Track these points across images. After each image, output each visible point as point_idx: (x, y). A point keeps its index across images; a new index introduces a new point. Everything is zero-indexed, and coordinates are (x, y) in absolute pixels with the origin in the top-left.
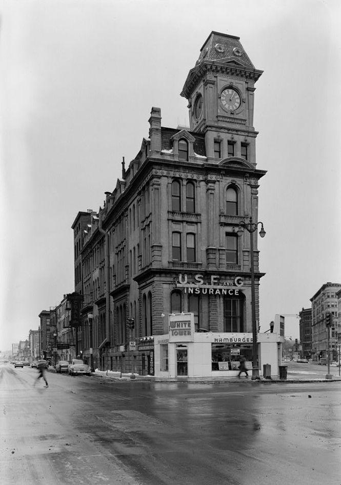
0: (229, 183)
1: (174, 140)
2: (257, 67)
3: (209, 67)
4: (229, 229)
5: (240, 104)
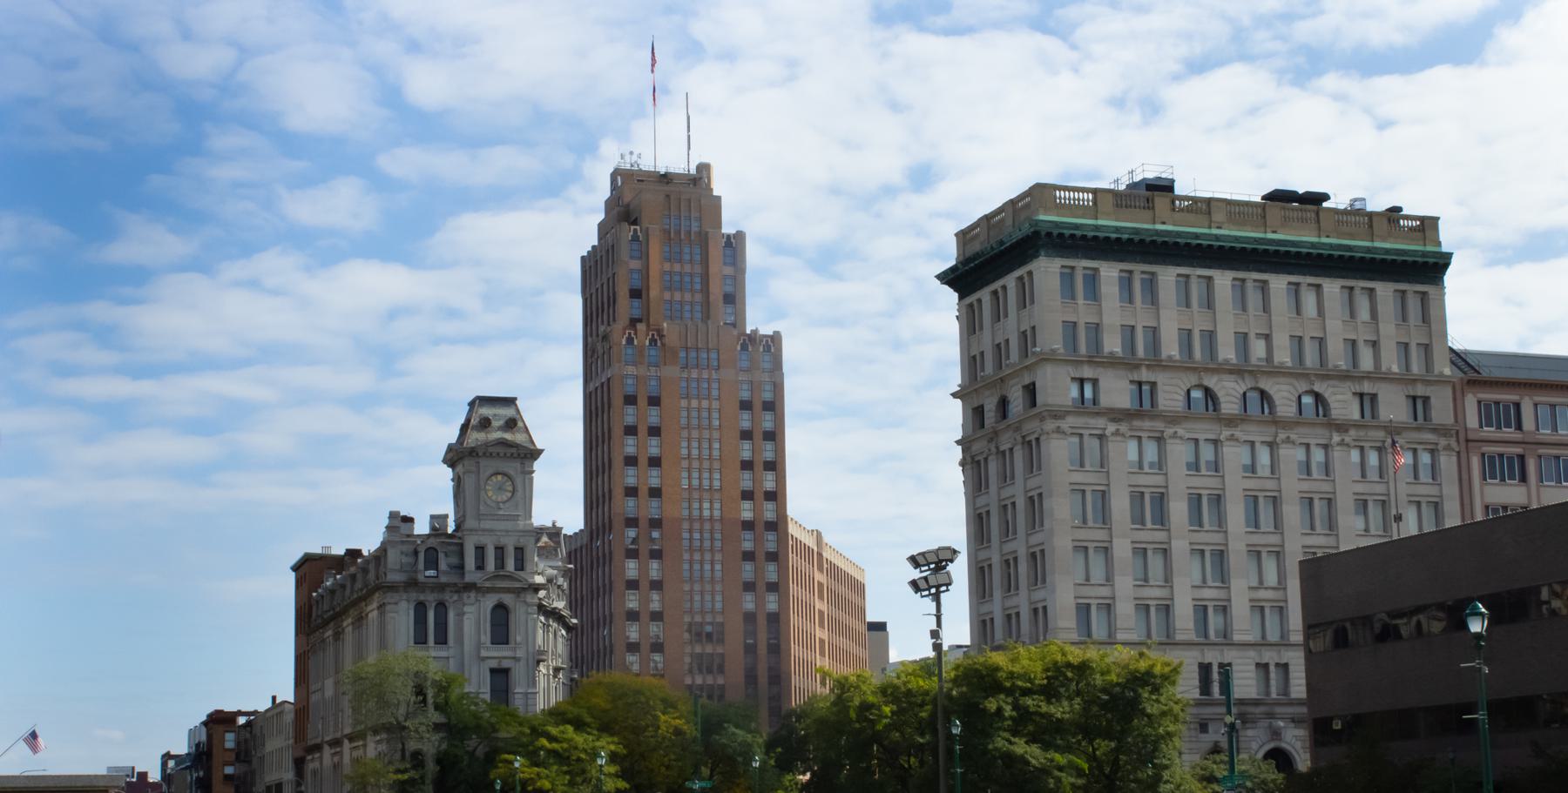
2: (539, 446)
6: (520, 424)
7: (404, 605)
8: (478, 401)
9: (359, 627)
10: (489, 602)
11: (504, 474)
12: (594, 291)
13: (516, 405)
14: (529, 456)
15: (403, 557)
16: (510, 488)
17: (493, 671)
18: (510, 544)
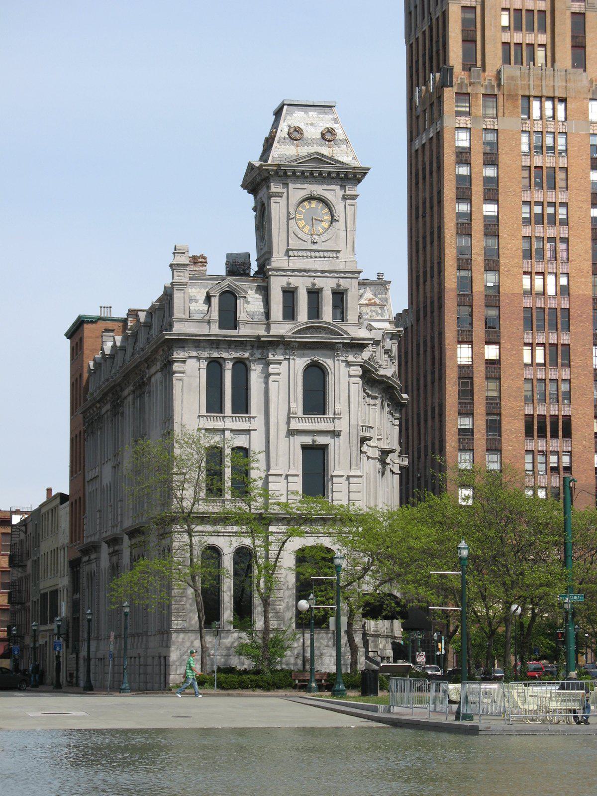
9: (140, 396)
10: (300, 363)
12: (420, 35)
16: (328, 217)
17: (305, 447)
18: (327, 285)
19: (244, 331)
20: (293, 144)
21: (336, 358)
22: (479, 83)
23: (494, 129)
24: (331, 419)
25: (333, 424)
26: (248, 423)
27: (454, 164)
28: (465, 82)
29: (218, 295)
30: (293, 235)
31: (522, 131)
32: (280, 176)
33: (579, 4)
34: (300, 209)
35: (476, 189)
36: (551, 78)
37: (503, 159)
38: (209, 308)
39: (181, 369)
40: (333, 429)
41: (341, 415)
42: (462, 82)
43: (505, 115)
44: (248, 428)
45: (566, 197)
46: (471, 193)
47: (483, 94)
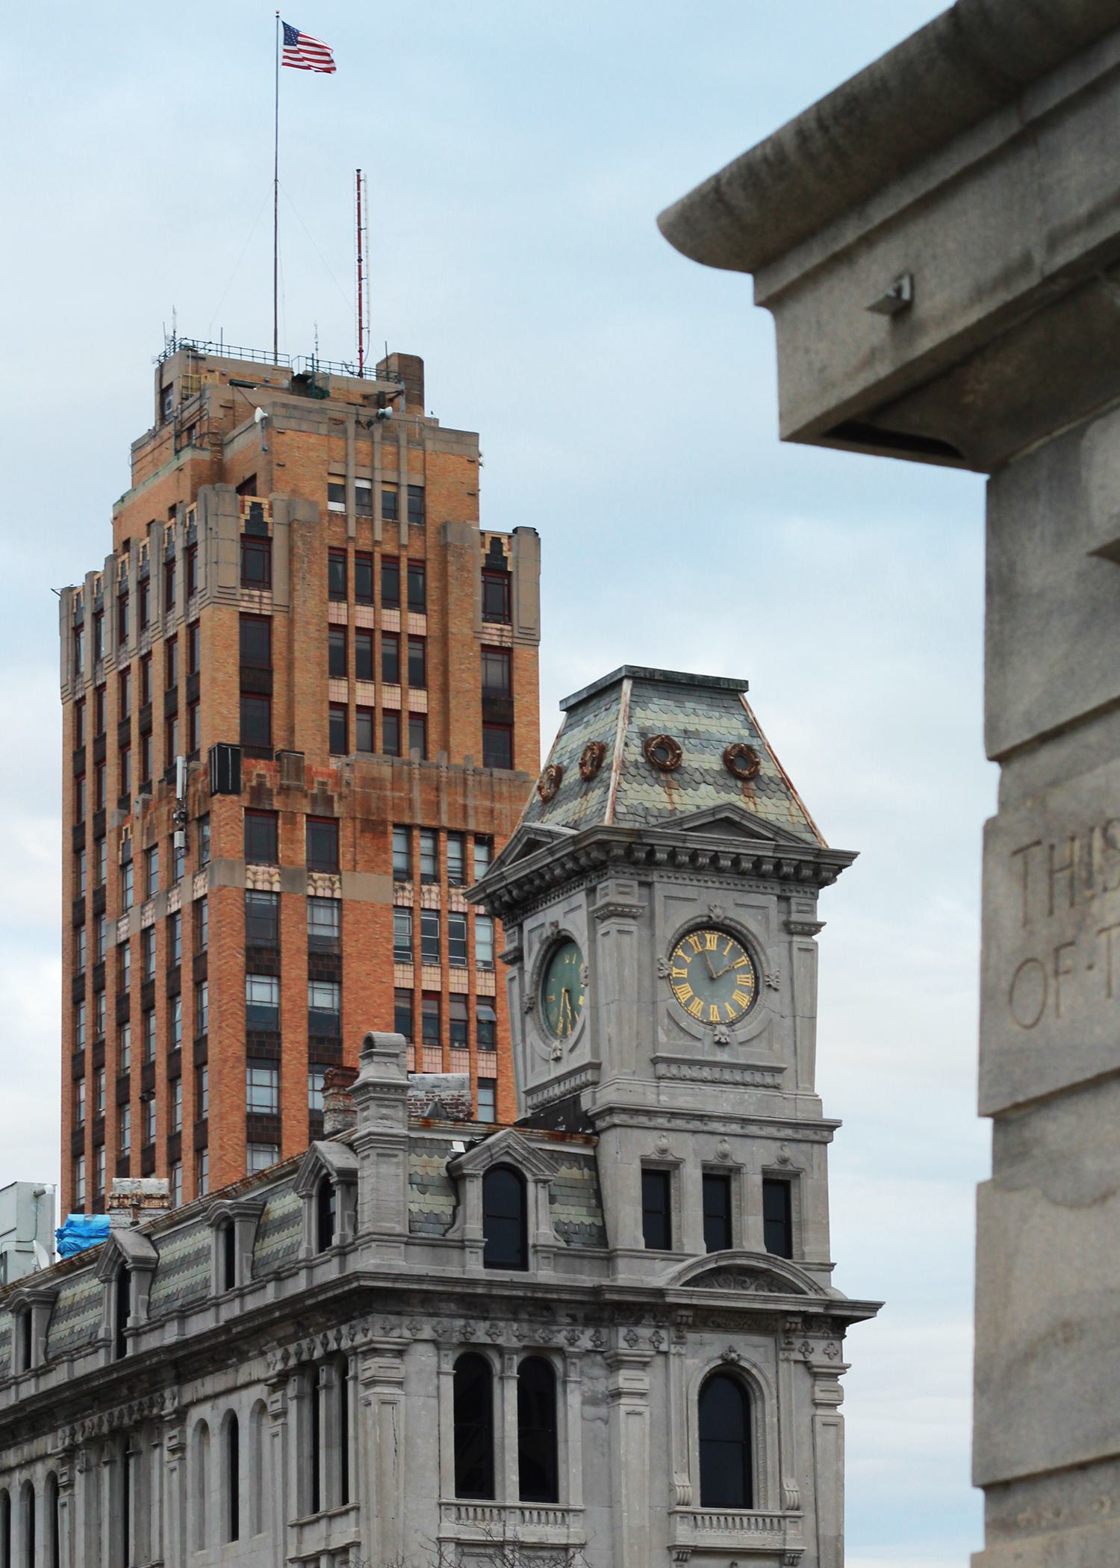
0: (710, 1361)
1: (464, 1177)
2: (834, 840)
3: (619, 852)
4: (544, 1255)
5: (757, 993)
6: (766, 769)
7: (423, 1358)
8: (627, 685)
11: (727, 930)
13: (744, 708)
14: (807, 872)
15: (415, 1194)
19: (542, 1273)
20: (657, 781)
21: (781, 1356)
22: (299, 789)
23: (332, 899)
24: (775, 1520)
25: (779, 1537)
26: (565, 1530)
27: (241, 975)
28: (268, 785)
29: (482, 1173)
30: (666, 1021)
31: (396, 906)
32: (636, 863)
33: (499, 626)
34: (680, 952)
35: (291, 1037)
36: (460, 790)
37: (353, 969)
38: (455, 1208)
39: (394, 1375)
40: (778, 1547)
41: (798, 1509)
42: (261, 785)
43: (359, 868)
44: (564, 1541)
45: (493, 1065)
46: (280, 1045)
47: (308, 816)
